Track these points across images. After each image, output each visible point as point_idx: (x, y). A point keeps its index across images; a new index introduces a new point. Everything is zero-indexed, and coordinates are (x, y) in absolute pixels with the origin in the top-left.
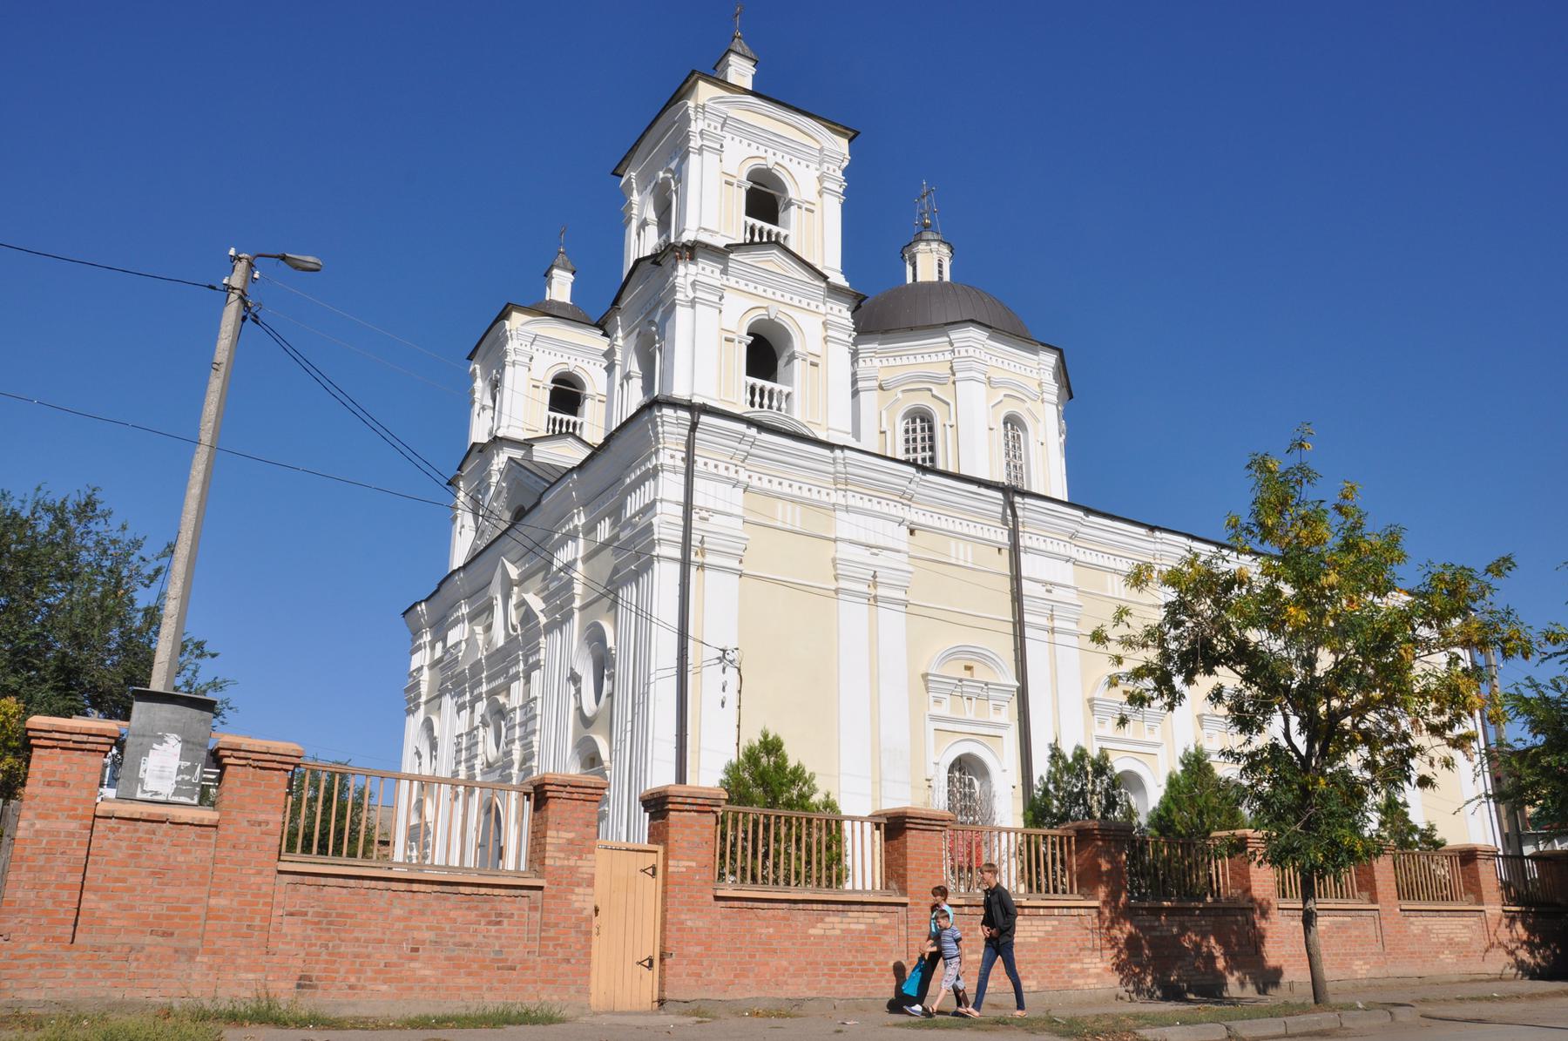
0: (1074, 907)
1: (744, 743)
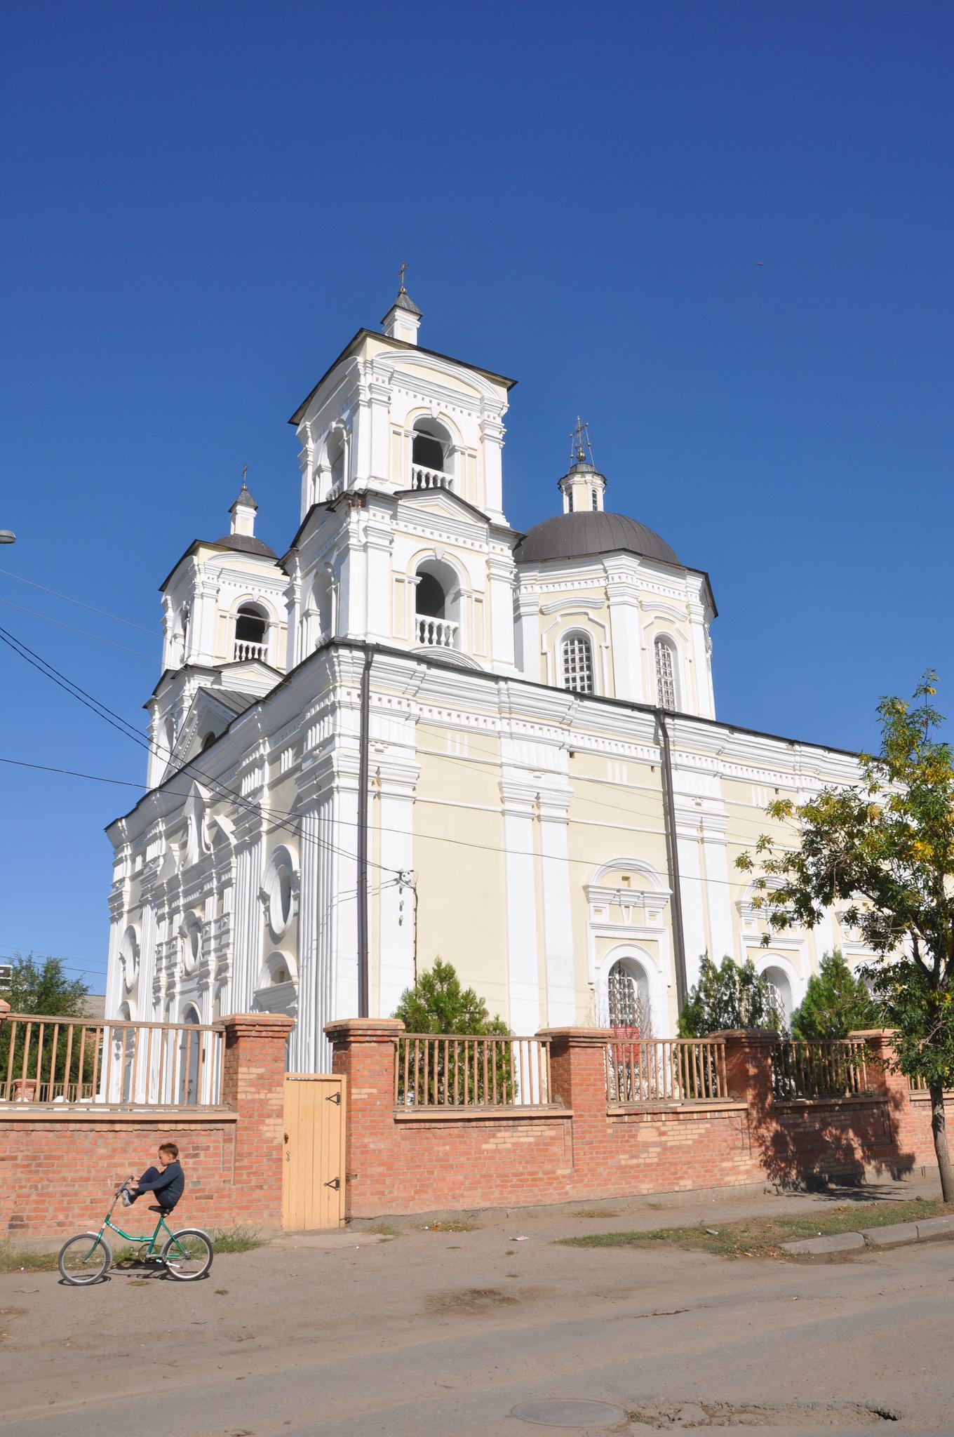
0: (724, 1111)
1: (420, 972)
